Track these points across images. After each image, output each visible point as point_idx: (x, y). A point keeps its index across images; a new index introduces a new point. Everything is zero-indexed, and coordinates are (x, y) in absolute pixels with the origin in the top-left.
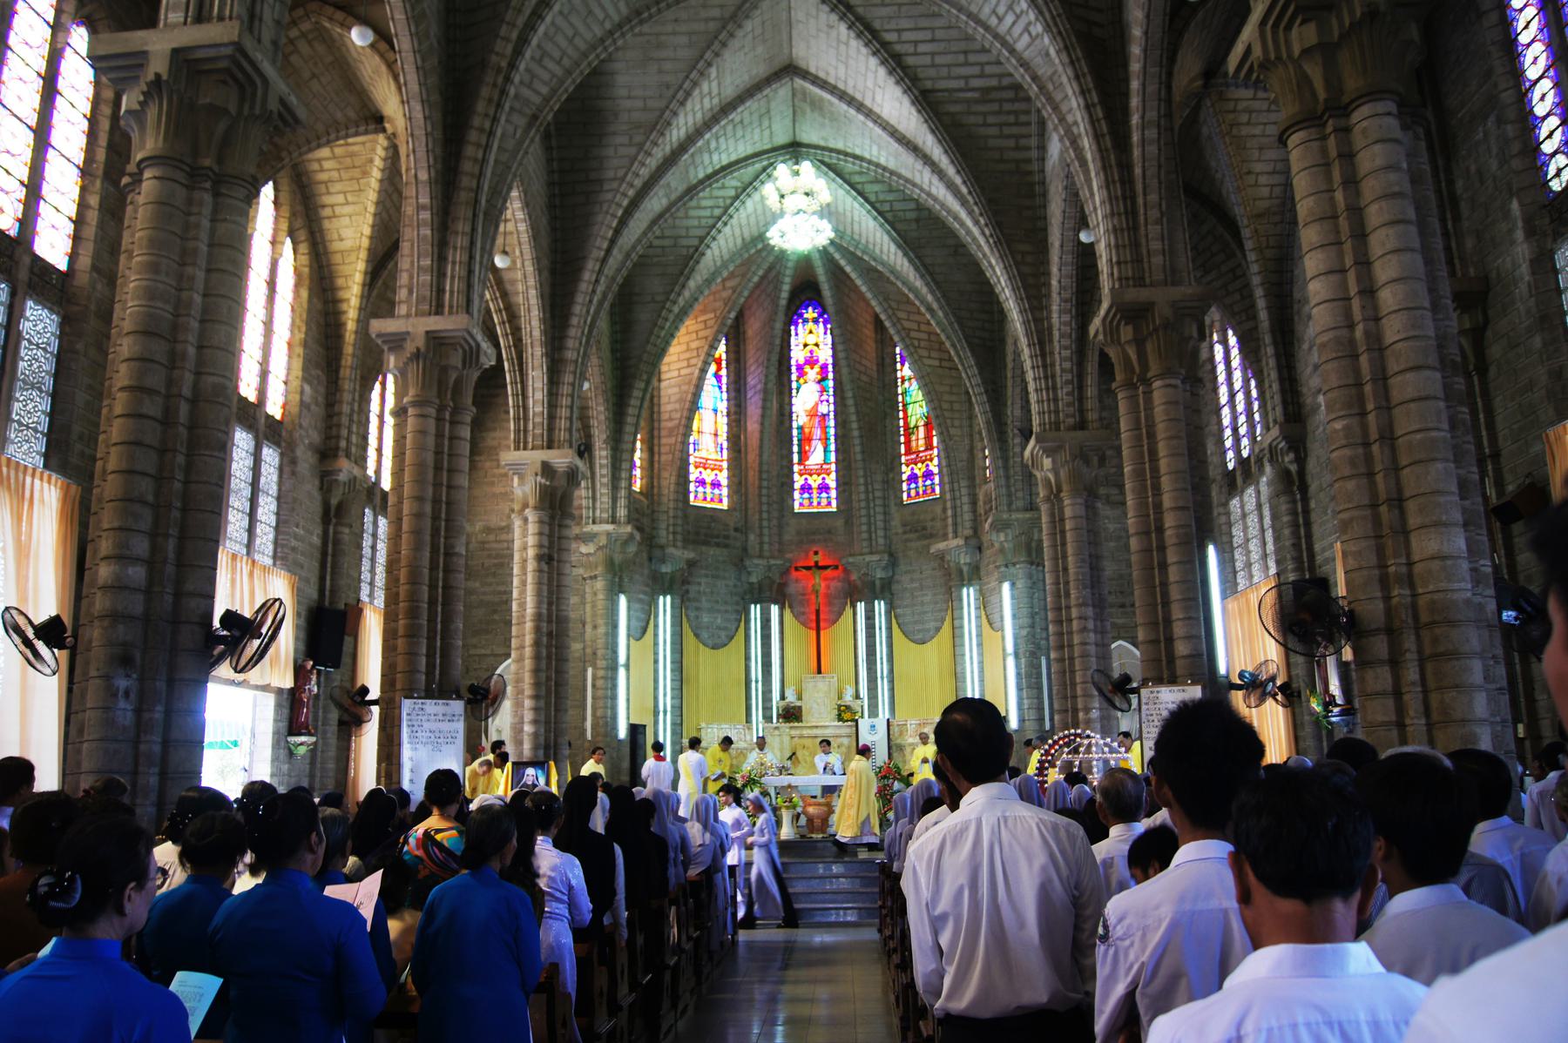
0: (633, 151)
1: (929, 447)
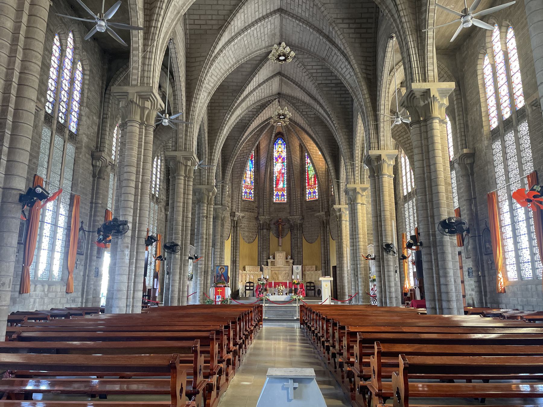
0: (233, 98)
1: (315, 184)
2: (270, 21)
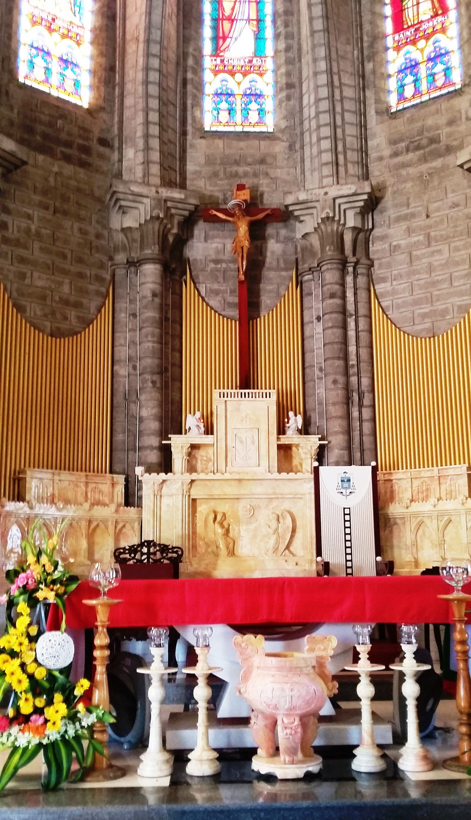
2: (103, 731)
